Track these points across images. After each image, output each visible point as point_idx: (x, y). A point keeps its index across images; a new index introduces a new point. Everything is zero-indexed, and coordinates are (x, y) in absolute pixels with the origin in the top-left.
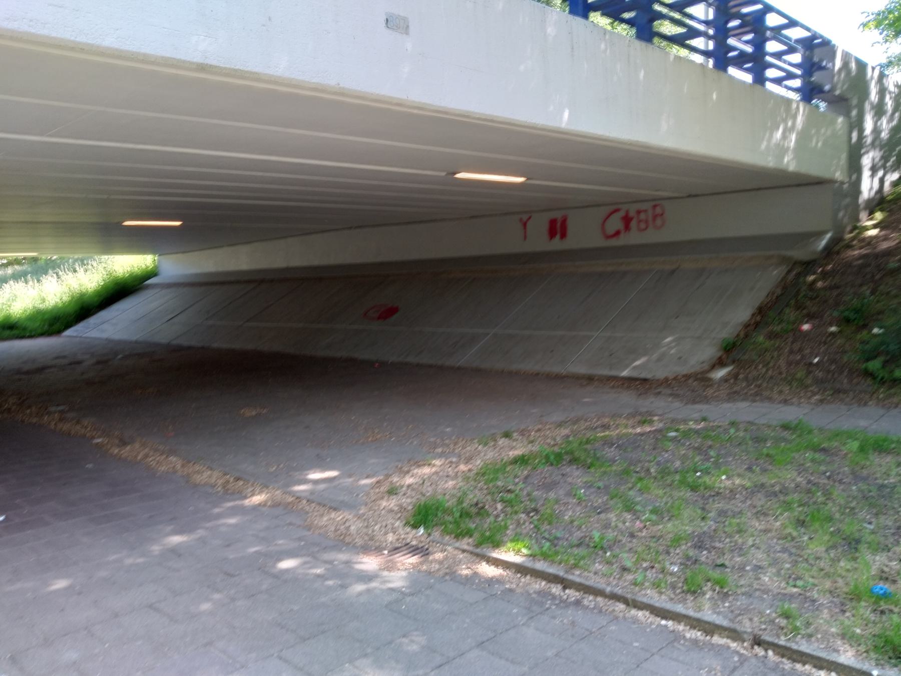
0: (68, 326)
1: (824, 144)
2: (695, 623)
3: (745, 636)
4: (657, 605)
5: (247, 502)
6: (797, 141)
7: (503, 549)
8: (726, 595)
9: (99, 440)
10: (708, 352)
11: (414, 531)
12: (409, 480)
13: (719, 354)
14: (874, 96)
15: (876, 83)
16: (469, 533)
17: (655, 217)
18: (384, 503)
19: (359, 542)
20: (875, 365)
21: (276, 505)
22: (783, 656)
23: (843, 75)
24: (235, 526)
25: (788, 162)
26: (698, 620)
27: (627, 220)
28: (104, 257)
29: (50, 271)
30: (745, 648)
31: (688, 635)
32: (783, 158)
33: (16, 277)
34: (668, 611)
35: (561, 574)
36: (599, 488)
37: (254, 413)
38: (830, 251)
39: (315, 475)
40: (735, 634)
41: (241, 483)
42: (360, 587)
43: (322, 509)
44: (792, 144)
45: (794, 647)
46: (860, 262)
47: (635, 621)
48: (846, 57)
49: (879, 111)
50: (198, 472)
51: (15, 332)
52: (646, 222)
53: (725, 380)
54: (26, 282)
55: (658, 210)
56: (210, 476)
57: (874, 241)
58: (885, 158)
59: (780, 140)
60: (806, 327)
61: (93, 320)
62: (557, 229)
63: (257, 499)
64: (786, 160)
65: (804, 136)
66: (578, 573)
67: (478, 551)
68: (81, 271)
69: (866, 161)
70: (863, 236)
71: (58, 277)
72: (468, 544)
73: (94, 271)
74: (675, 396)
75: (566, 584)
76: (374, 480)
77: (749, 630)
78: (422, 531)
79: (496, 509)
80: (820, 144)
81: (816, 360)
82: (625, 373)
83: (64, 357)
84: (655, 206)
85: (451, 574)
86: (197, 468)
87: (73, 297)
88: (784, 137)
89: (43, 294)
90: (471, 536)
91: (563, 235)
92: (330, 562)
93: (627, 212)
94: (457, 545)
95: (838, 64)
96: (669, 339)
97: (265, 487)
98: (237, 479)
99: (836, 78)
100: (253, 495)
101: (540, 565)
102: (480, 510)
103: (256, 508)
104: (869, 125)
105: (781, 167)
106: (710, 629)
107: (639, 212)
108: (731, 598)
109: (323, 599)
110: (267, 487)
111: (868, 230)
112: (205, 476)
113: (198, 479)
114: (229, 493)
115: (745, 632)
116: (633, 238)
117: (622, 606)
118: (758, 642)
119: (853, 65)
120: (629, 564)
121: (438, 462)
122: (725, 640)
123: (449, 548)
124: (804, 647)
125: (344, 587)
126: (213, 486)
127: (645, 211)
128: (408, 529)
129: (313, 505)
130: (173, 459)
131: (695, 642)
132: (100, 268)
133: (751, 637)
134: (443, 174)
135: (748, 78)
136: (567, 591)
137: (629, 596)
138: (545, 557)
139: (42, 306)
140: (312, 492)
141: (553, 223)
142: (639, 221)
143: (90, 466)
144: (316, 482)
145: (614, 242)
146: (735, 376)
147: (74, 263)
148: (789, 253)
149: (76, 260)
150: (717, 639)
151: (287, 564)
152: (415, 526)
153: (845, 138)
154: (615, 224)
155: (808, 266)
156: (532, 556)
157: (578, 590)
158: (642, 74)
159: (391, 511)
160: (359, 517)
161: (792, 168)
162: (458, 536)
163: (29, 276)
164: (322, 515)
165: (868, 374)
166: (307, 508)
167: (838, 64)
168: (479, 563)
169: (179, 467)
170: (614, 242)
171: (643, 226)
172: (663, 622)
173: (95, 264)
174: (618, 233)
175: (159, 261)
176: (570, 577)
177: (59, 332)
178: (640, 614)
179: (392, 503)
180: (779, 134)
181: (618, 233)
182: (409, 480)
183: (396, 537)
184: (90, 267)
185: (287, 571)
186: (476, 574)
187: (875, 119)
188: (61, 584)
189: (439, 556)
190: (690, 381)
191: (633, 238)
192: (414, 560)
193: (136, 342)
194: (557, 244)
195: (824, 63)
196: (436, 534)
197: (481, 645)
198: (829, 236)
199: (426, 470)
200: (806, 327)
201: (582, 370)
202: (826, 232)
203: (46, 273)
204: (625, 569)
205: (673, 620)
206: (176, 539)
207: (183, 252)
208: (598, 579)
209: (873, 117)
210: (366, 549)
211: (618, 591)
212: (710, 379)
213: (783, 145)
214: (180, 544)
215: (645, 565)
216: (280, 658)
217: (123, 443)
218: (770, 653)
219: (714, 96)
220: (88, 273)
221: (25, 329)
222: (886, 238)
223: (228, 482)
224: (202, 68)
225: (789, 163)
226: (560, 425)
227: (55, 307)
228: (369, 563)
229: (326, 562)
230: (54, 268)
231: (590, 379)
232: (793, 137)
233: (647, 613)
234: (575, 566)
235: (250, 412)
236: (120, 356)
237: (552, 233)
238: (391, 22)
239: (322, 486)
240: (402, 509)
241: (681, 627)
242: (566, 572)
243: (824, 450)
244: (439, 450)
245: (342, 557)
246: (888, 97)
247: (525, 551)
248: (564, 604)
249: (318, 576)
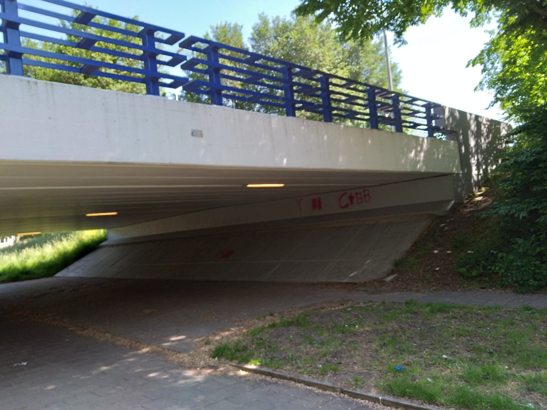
0: (58, 271)
1: (443, 156)
2: (320, 386)
3: (338, 389)
4: (306, 380)
5: (140, 352)
6: (424, 157)
7: (250, 363)
8: (336, 374)
9: (72, 328)
10: (388, 267)
11: (214, 359)
12: (217, 338)
13: (393, 267)
14: (473, 127)
15: (474, 121)
16: (236, 358)
17: (365, 196)
18: (203, 349)
19: (188, 365)
20: (463, 270)
21: (153, 352)
22: (351, 396)
23: (451, 120)
24: (133, 362)
25: (420, 168)
26: (321, 385)
27: (351, 198)
28: (78, 232)
29: (48, 241)
30: (337, 395)
31: (316, 391)
32: (417, 166)
33: (29, 245)
34: (310, 383)
35: (271, 371)
36: (301, 335)
37: (150, 311)
38: (454, 209)
39: (174, 339)
40: (333, 389)
41: (138, 344)
42: (182, 382)
43: (173, 353)
44: (422, 158)
45: (354, 391)
46: (469, 215)
47: (297, 388)
48: (452, 111)
49: (478, 134)
50: (119, 340)
51: (29, 276)
52: (361, 199)
53: (392, 281)
54: (35, 248)
55: (367, 193)
56: (124, 342)
57: (480, 202)
58: (485, 159)
59: (414, 157)
60: (436, 252)
61: (71, 267)
62: (317, 204)
63: (145, 350)
64: (418, 167)
65: (428, 154)
66: (278, 370)
67: (239, 365)
68: (64, 240)
69: (473, 161)
70: (474, 200)
71: (52, 244)
72: (236, 363)
73: (72, 239)
74: (365, 291)
75: (272, 375)
76: (201, 339)
77: (339, 387)
78: (216, 359)
79: (252, 347)
80: (440, 156)
81: (437, 269)
82: (346, 281)
83: (56, 288)
84: (364, 191)
85: (225, 375)
86: (119, 338)
87: (60, 255)
88: (416, 155)
89: (44, 254)
90: (237, 360)
91: (320, 207)
92: (172, 374)
93: (351, 194)
94: (231, 364)
95: (447, 114)
96: (368, 261)
97: (149, 345)
98: (137, 342)
99: (446, 123)
100: (143, 348)
101: (264, 369)
102: (245, 348)
103: (144, 354)
104: (472, 143)
105: (415, 170)
106: (325, 388)
107: (357, 194)
108: (337, 376)
109: (165, 387)
110: (150, 345)
111: (477, 197)
112: (122, 341)
113: (118, 343)
114: (132, 348)
115: (338, 388)
116: (355, 208)
117: (293, 382)
118: (343, 392)
119: (457, 114)
120: (300, 365)
121: (233, 329)
122: (331, 392)
123: (227, 365)
124: (358, 391)
125: (175, 382)
126: (125, 346)
127: (360, 193)
128: (211, 359)
129: (170, 351)
130: (107, 335)
131: (318, 394)
132: (75, 238)
133: (340, 390)
134: (241, 186)
135: (393, 128)
136: (273, 379)
137: (296, 378)
138: (266, 365)
139: (43, 261)
140: (170, 346)
141: (314, 201)
142: (358, 198)
143: (67, 340)
144: (173, 341)
145: (345, 210)
146: (397, 279)
147: (61, 236)
148: (432, 212)
149: (62, 234)
150: (327, 392)
151: (152, 375)
152: (214, 357)
153: (457, 151)
154: (345, 200)
155: (442, 218)
156: (261, 366)
157: (277, 378)
158: (325, 138)
159: (206, 352)
160: (189, 355)
161: (423, 170)
162: (232, 360)
163: (36, 245)
164: (173, 355)
165: (461, 275)
166: (167, 353)
167: (447, 114)
168: (239, 371)
169: (110, 338)
170: (345, 210)
171: (360, 201)
172: (308, 387)
173: (72, 236)
174: (347, 205)
175: (107, 232)
176: (275, 372)
177: (52, 275)
178: (299, 385)
179: (207, 348)
180: (412, 154)
181: (347, 205)
182: (217, 338)
183: (204, 362)
184: (69, 238)
185: (152, 377)
186: (236, 375)
187: (476, 139)
188: (51, 387)
189: (222, 369)
190: (375, 283)
191: (355, 208)
192: (209, 371)
193: (94, 278)
194: (317, 212)
195: (438, 116)
196: (223, 360)
197: (226, 399)
198: (453, 202)
199: (227, 333)
200: (436, 252)
201: (324, 280)
202: (452, 200)
203: (46, 242)
204: (299, 368)
205: (312, 386)
206: (104, 368)
207: (121, 227)
208: (286, 372)
209: (475, 138)
210: (190, 368)
211: (292, 376)
212: (385, 281)
213: (416, 160)
214: (106, 370)
215: (308, 365)
216: (142, 407)
217: (84, 329)
218: (346, 395)
219: (369, 142)
220: (69, 241)
221: (34, 274)
222: (485, 201)
223: (132, 344)
224: (110, 163)
225: (420, 167)
226: (301, 308)
227: (51, 261)
228: (190, 373)
229: (170, 373)
230: (50, 240)
231: (327, 284)
232: (422, 154)
233: (303, 385)
234: (278, 368)
235: (147, 311)
236: (85, 286)
237: (314, 207)
238: (193, 134)
239: (174, 344)
240: (210, 350)
241: (314, 389)
242: (273, 370)
243: (416, 313)
244: (237, 324)
245: (178, 371)
246: (483, 127)
247: (258, 363)
248: (270, 383)
249: (165, 379)
